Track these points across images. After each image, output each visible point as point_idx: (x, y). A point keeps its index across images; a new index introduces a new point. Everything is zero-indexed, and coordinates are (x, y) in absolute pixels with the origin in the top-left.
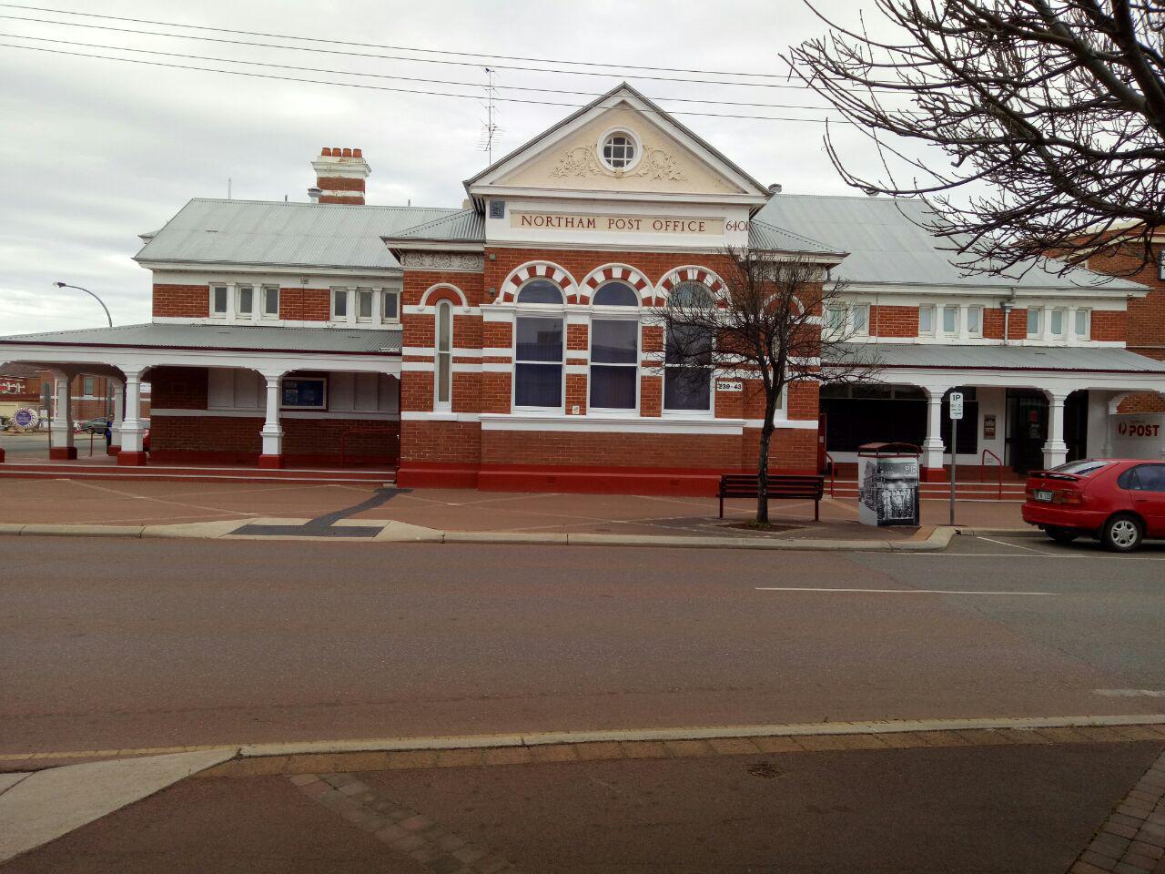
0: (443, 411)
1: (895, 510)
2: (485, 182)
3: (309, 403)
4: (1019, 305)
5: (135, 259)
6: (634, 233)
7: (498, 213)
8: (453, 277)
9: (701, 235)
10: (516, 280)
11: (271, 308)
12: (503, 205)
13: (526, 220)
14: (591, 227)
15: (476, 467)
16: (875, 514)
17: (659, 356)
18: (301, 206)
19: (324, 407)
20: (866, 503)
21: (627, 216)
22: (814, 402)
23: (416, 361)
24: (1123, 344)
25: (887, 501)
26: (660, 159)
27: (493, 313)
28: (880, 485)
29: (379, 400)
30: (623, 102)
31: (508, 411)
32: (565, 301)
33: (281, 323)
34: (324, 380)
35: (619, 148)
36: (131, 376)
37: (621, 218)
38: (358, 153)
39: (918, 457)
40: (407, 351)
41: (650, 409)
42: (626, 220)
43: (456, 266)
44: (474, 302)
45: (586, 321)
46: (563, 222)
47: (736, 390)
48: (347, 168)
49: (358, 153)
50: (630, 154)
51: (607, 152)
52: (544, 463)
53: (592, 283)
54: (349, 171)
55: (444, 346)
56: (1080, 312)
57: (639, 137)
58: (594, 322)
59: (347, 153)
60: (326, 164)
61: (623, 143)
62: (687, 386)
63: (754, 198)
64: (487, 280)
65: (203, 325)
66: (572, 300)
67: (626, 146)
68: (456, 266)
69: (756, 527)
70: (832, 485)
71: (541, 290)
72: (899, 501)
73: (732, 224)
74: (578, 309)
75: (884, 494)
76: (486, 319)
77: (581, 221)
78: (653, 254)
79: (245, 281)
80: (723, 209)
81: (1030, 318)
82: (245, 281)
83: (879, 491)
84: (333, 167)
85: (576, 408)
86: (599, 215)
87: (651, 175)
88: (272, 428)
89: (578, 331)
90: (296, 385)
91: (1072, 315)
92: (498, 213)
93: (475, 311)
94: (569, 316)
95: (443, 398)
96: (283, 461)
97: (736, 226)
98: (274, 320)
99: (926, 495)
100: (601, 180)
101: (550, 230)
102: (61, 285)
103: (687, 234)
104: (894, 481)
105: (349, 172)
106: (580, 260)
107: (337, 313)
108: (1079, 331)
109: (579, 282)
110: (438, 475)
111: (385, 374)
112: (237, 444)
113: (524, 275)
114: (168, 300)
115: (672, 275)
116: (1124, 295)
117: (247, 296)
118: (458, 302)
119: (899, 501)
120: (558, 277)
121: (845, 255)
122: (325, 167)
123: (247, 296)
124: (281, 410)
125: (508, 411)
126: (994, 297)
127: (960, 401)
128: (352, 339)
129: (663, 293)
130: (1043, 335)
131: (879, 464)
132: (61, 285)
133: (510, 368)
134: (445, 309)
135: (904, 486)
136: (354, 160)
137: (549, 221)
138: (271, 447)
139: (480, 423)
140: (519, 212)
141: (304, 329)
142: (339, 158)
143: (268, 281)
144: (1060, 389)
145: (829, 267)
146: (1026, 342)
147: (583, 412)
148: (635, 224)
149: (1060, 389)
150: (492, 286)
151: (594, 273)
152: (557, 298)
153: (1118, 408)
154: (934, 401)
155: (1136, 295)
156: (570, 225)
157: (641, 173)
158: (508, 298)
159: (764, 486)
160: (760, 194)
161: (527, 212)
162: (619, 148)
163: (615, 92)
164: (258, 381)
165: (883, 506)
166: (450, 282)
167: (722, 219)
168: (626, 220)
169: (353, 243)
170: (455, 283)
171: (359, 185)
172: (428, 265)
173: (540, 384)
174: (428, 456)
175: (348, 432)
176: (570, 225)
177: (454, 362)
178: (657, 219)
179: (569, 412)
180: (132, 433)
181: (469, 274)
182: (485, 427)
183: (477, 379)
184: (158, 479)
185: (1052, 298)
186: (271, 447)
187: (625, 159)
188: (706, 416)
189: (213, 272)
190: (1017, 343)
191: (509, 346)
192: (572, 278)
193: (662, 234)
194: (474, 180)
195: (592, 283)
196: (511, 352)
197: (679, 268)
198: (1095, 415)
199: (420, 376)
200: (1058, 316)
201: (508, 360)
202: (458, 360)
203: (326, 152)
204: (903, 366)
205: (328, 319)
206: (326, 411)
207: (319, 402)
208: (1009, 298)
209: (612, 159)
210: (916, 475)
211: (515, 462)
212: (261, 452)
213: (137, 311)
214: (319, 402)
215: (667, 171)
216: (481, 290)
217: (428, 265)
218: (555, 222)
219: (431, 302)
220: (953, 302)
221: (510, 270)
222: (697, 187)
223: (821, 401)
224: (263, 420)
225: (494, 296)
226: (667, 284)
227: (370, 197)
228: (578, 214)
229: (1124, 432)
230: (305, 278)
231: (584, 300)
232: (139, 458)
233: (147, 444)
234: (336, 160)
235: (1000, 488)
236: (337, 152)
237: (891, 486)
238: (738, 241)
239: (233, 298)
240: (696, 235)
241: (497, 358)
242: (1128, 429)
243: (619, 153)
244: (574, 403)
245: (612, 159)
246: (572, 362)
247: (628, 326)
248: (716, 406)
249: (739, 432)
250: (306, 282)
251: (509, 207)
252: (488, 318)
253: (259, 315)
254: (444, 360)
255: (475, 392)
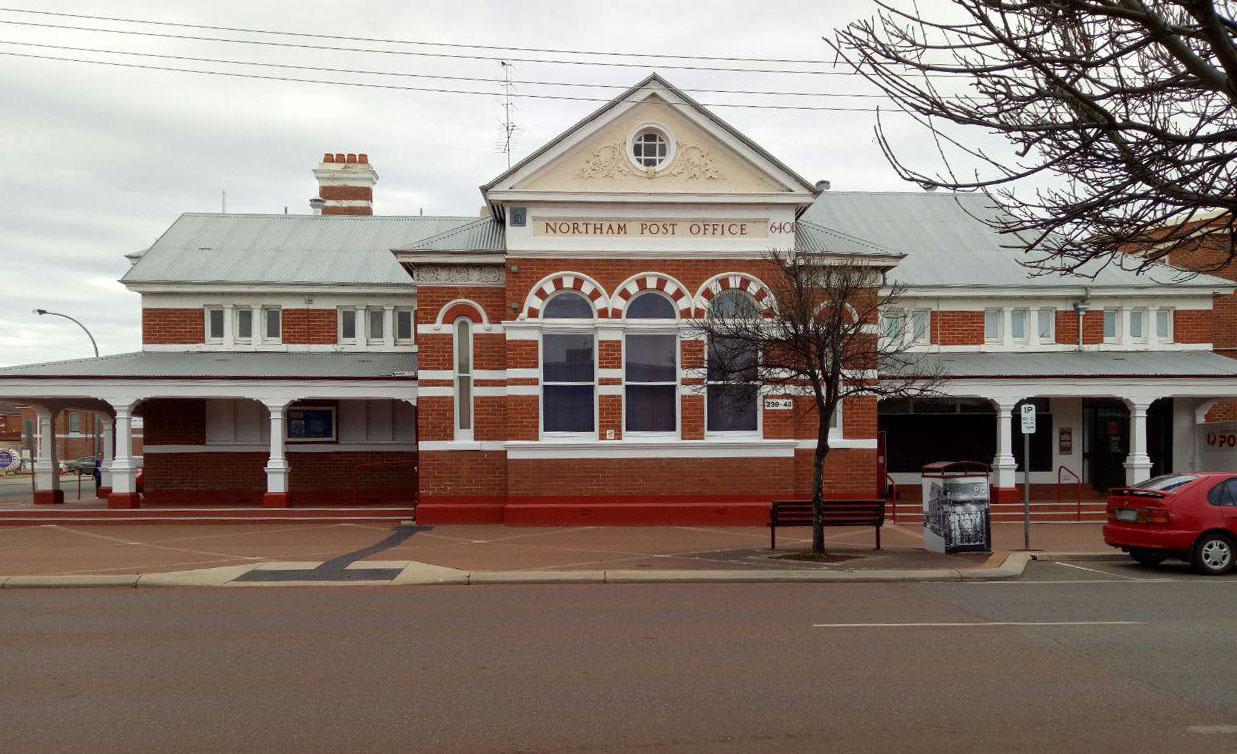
0: (464, 440)
1: (964, 535)
2: (504, 186)
3: (317, 435)
4: (1094, 307)
5: (122, 281)
6: (669, 238)
7: (519, 220)
8: (471, 292)
9: (743, 239)
10: (541, 294)
11: (272, 332)
12: (524, 212)
13: (550, 227)
14: (622, 233)
15: (501, 501)
16: (942, 540)
17: (700, 373)
18: (302, 218)
19: (334, 439)
20: (932, 528)
21: (661, 220)
22: (872, 419)
23: (435, 385)
24: (1209, 347)
25: (955, 526)
26: (695, 156)
27: (517, 331)
28: (947, 508)
29: (394, 429)
30: (654, 95)
31: (536, 438)
32: (596, 314)
33: (284, 348)
34: (333, 408)
35: (650, 146)
36: (120, 411)
37: (654, 222)
38: (363, 159)
39: (987, 476)
40: (423, 375)
41: (692, 431)
42: (660, 225)
43: (475, 279)
44: (495, 319)
45: (619, 336)
46: (591, 228)
47: (786, 408)
48: (353, 176)
49: (363, 159)
50: (663, 152)
51: (637, 150)
52: (577, 493)
53: (625, 294)
54: (354, 178)
55: (463, 368)
56: (1161, 313)
57: (672, 133)
58: (627, 336)
59: (352, 159)
60: (328, 171)
61: (655, 140)
62: (732, 406)
63: (800, 196)
64: (509, 294)
65: (199, 353)
66: (603, 313)
67: (658, 143)
68: (475, 279)
69: (812, 558)
70: (894, 510)
71: (569, 304)
72: (968, 525)
73: (777, 225)
74: (610, 323)
75: (951, 518)
76: (509, 337)
77: (610, 227)
78: (690, 261)
79: (243, 302)
80: (766, 209)
81: (1107, 320)
82: (243, 302)
83: (946, 515)
84: (337, 175)
85: (610, 433)
86: (630, 220)
87: (685, 175)
88: (277, 463)
89: (611, 347)
90: (302, 416)
91: (1153, 316)
92: (519, 220)
93: (497, 329)
94: (600, 332)
95: (464, 425)
96: (290, 499)
97: (781, 228)
98: (276, 344)
99: (999, 518)
100: (632, 181)
101: (577, 238)
102: (41, 312)
103: (728, 238)
104: (962, 503)
105: (354, 179)
106: (611, 270)
107: (213, 335)
108: (1161, 333)
109: (610, 293)
110: (461, 511)
111: (399, 400)
112: (238, 483)
113: (549, 288)
114: (160, 325)
115: (712, 283)
116: (1209, 292)
117: (246, 317)
118: (478, 319)
119: (968, 525)
120: (587, 289)
121: (901, 257)
122: (328, 175)
123: (246, 317)
124: (286, 443)
125: (536, 438)
126: (1067, 298)
127: (1033, 414)
128: (362, 362)
129: (702, 303)
130: (1121, 338)
131: (945, 485)
132: (41, 312)
133: (537, 391)
134: (463, 327)
135: (973, 508)
136: (360, 166)
137: (576, 228)
138: (277, 484)
139: (506, 452)
140: (542, 219)
141: (309, 353)
142: (343, 165)
143: (268, 302)
144: (1141, 397)
145: (884, 270)
146: (1102, 347)
147: (618, 436)
148: (670, 229)
149: (1141, 397)
150: (514, 300)
151: (589, 281)
152: (588, 313)
153: (1206, 417)
154: (273, 416)
155: (1222, 292)
156: (598, 231)
157: (675, 172)
158: (533, 313)
159: (820, 512)
160: (806, 192)
161: (551, 219)
162: (650, 146)
163: (644, 84)
164: (261, 412)
165: (950, 531)
166: (469, 298)
167: (766, 221)
168: (660, 225)
169: (360, 258)
170: (474, 299)
171: (366, 194)
172: (443, 280)
173: (570, 407)
174: (450, 490)
175: (361, 466)
176: (598, 231)
177: (475, 385)
178: (694, 223)
179: (603, 437)
180: (123, 473)
181: (491, 289)
182: (511, 455)
183: (501, 403)
184: (153, 522)
185: (1130, 297)
186: (277, 484)
187: (657, 158)
188: (754, 437)
189: (208, 294)
190: (1093, 348)
191: (536, 366)
192: (602, 290)
193: (700, 238)
194: (492, 185)
195: (625, 294)
196: (538, 373)
197: (720, 276)
198: (1181, 425)
199: (438, 402)
200: (1137, 317)
201: (534, 382)
202: (480, 383)
203: (329, 158)
204: (969, 377)
205: (335, 342)
206: (336, 443)
207: (328, 433)
208: (1083, 299)
209: (643, 157)
210: (985, 495)
211: (545, 494)
212: (266, 490)
213: (126, 338)
214: (328, 433)
215: (703, 169)
216: (503, 306)
217: (443, 280)
218: (582, 228)
219: (447, 320)
220: (1022, 305)
221: (533, 283)
222: (738, 186)
223: (1037, 416)
224: (266, 456)
225: (521, 310)
226: (707, 294)
227: (378, 206)
228: (607, 220)
229: (1213, 443)
230: (310, 297)
231: (617, 314)
232: (132, 500)
233: (140, 484)
234: (339, 166)
235: (1079, 508)
236: (340, 158)
237: (959, 509)
238: (784, 244)
239: (230, 322)
240: (738, 239)
241: (493, 385)
242: (1218, 439)
243: (651, 151)
244: (608, 427)
245: (643, 157)
246: (605, 382)
247: (665, 341)
248: (764, 426)
249: (791, 454)
250: (310, 302)
251: (531, 213)
252: (511, 336)
253: (260, 339)
254: (464, 383)
255: (499, 418)
